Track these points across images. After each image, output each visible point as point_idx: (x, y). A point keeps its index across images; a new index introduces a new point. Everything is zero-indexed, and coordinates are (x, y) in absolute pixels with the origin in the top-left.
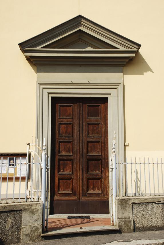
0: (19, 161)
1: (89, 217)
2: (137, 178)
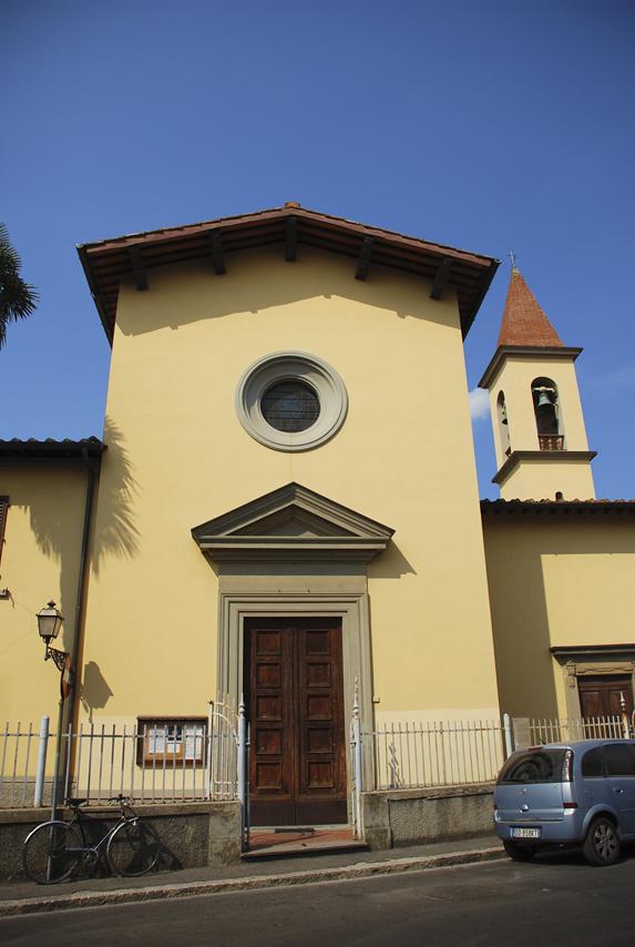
0: (189, 732)
1: (312, 830)
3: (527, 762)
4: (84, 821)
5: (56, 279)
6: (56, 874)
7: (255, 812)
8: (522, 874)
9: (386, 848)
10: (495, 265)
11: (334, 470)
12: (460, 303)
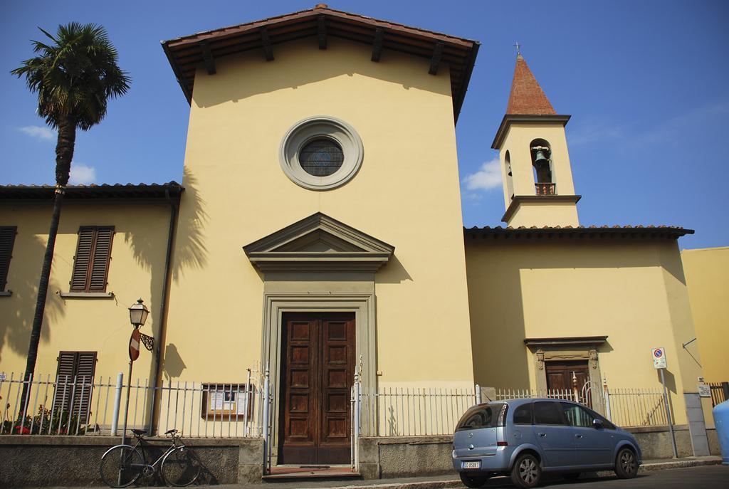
1: (329, 467)
2: (392, 418)
3: (475, 414)
4: (145, 447)
9: (375, 478)
10: (476, 47)
11: (352, 204)
12: (452, 77)
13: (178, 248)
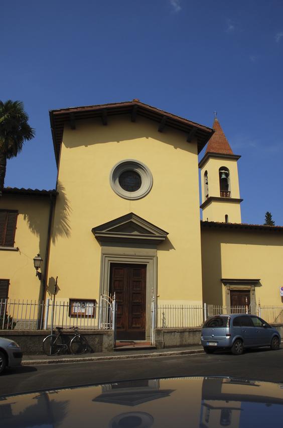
2: (164, 317)
5: (40, 125)
6: (53, 353)
7: (119, 335)
8: (210, 357)
11: (148, 208)
12: (198, 143)
13: (55, 226)
